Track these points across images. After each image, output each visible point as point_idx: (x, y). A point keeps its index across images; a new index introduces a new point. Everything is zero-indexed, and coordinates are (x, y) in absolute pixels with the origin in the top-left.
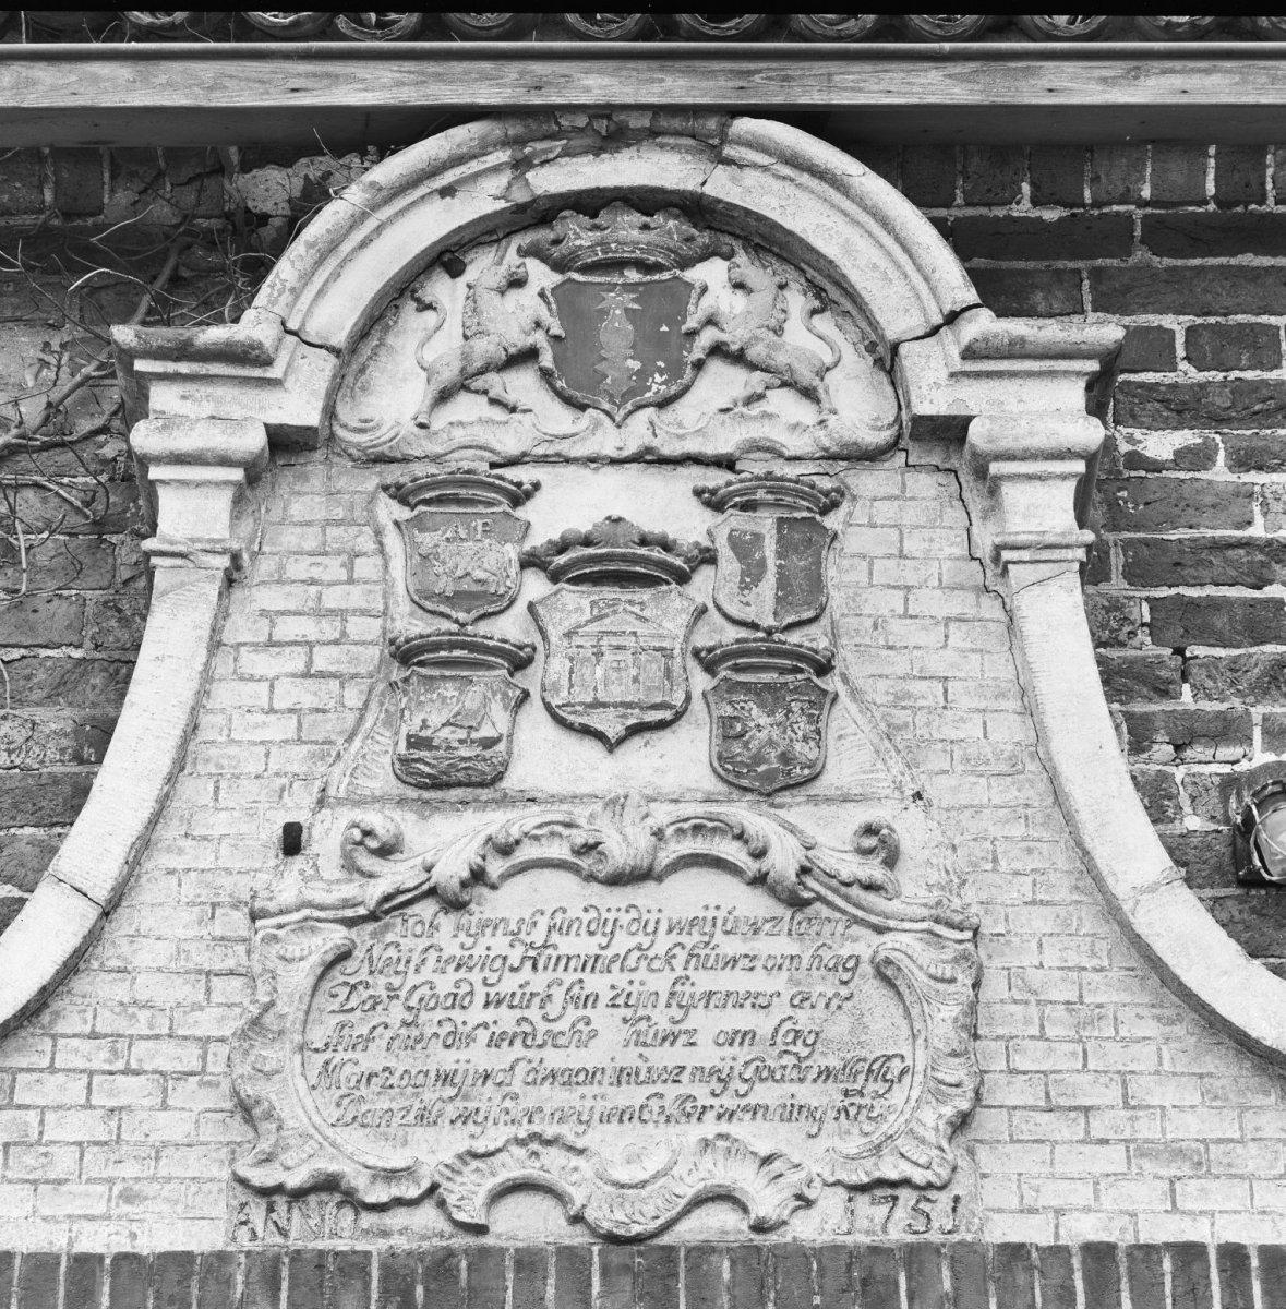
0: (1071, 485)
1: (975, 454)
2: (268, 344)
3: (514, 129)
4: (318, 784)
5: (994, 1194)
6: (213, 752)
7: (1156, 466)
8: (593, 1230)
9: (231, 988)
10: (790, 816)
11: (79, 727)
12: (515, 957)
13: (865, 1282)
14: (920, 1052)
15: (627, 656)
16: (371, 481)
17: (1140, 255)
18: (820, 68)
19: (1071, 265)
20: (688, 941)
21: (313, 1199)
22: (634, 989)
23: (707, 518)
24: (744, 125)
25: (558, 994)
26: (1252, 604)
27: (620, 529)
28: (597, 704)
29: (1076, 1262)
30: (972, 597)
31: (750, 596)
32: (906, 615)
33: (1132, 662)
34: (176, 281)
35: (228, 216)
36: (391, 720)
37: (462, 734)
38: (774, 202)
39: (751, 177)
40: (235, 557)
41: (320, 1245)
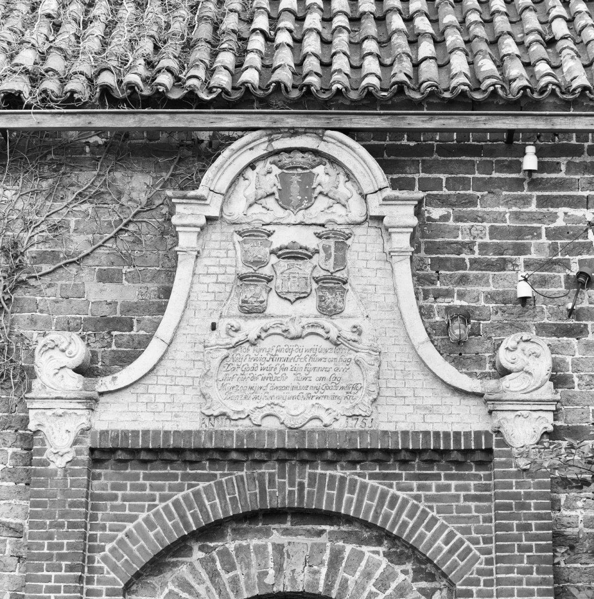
0: (409, 234)
1: (385, 226)
2: (206, 195)
3: (269, 132)
4: (220, 312)
5: (382, 418)
6: (194, 303)
7: (435, 220)
8: (286, 426)
9: (199, 364)
10: (335, 322)
11: (159, 289)
12: (268, 357)
13: (350, 440)
14: (365, 383)
15: (296, 279)
16: (232, 229)
17: (435, 156)
18: (349, 117)
19: (417, 159)
20: (310, 354)
21: (220, 417)
22: (297, 366)
23: (317, 241)
24: (328, 132)
25: (278, 367)
26: (457, 259)
27: (295, 245)
28: (288, 292)
29: (399, 435)
30: (383, 263)
31: (327, 263)
32: (366, 268)
33: (425, 275)
34: (180, 160)
35: (193, 140)
36: (238, 295)
37: (255, 300)
38: (336, 153)
39: (330, 145)
40: (198, 252)
41: (222, 429)
